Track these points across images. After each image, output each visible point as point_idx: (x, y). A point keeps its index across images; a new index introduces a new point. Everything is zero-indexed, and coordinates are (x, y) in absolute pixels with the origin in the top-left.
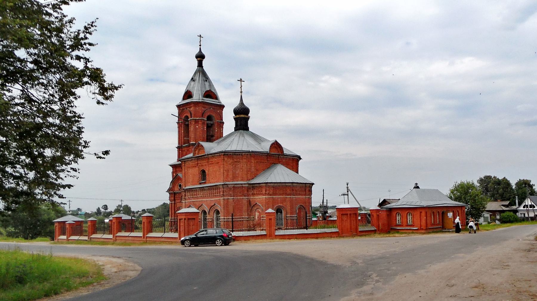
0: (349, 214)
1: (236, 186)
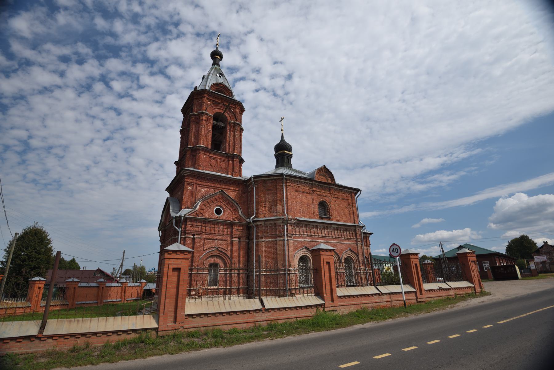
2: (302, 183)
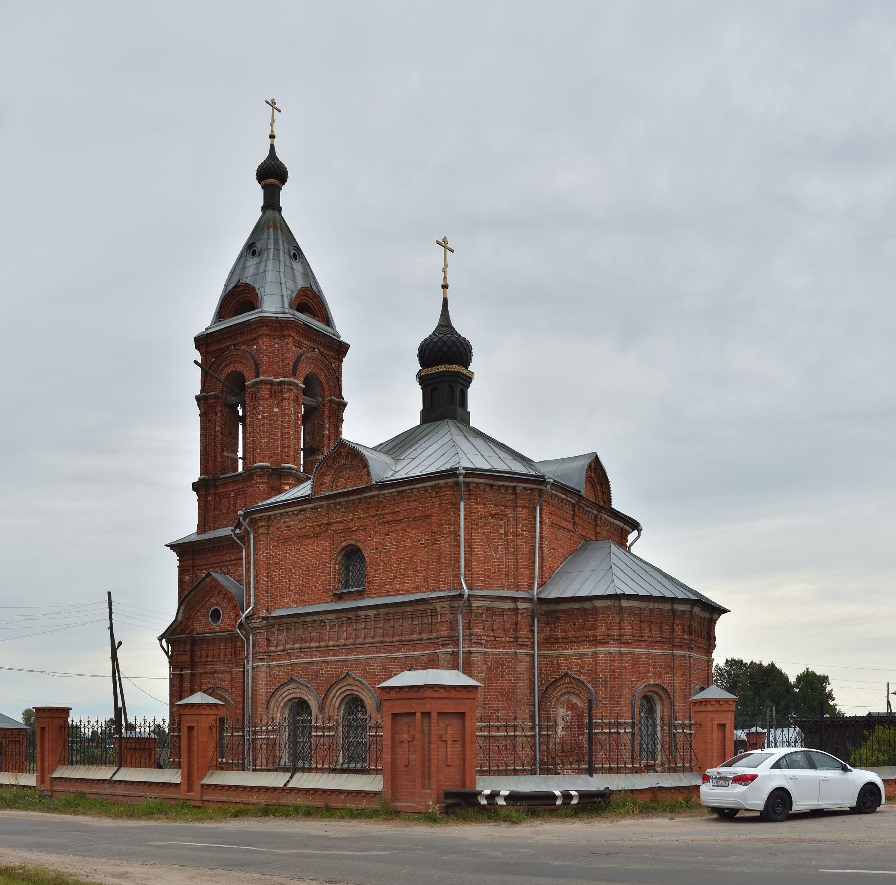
2: (293, 514)
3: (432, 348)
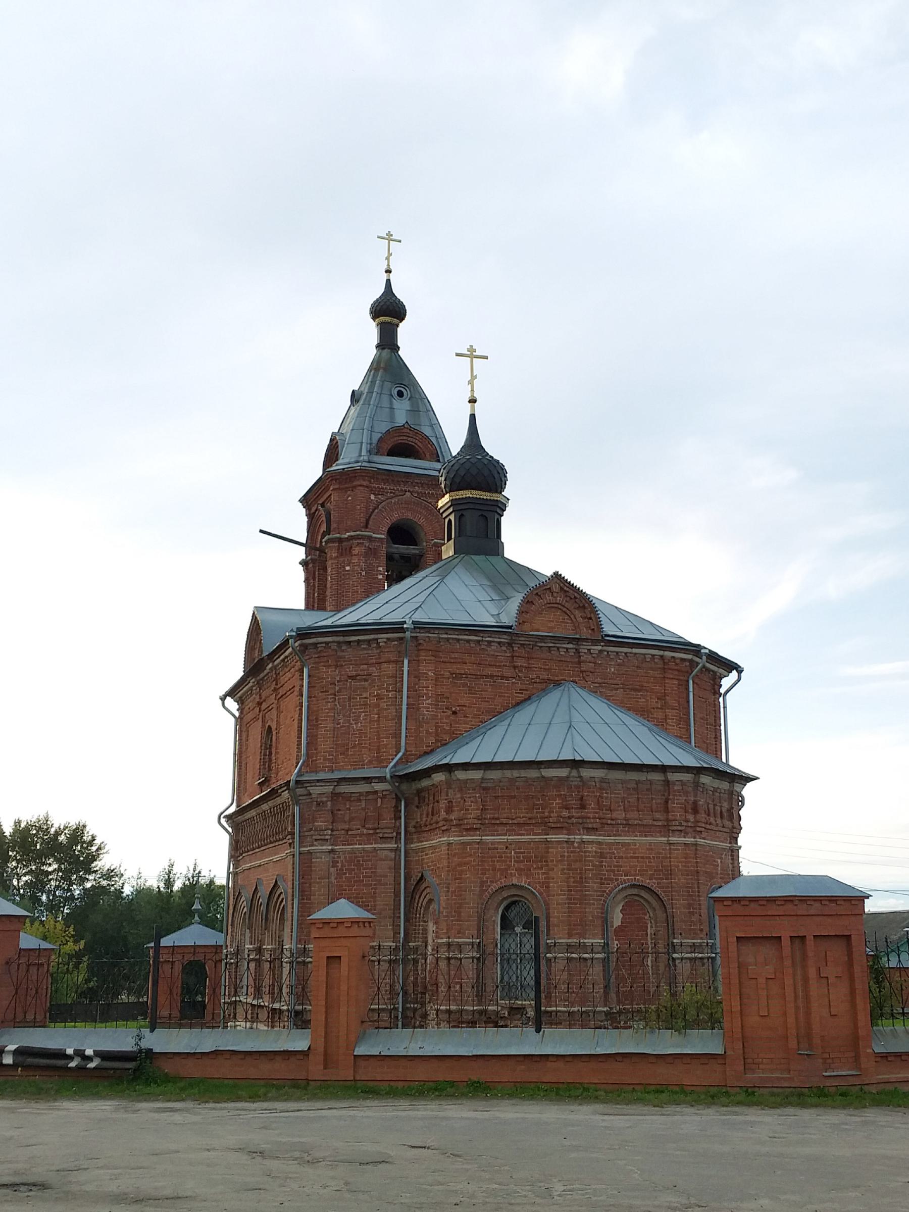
0: (786, 942)
1: (344, 789)
3: (463, 477)
